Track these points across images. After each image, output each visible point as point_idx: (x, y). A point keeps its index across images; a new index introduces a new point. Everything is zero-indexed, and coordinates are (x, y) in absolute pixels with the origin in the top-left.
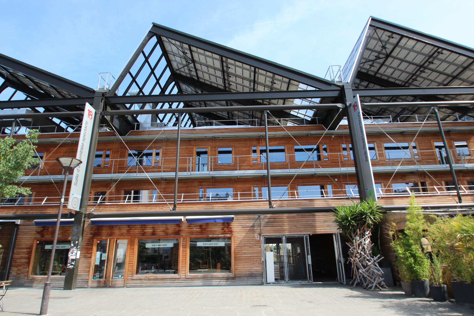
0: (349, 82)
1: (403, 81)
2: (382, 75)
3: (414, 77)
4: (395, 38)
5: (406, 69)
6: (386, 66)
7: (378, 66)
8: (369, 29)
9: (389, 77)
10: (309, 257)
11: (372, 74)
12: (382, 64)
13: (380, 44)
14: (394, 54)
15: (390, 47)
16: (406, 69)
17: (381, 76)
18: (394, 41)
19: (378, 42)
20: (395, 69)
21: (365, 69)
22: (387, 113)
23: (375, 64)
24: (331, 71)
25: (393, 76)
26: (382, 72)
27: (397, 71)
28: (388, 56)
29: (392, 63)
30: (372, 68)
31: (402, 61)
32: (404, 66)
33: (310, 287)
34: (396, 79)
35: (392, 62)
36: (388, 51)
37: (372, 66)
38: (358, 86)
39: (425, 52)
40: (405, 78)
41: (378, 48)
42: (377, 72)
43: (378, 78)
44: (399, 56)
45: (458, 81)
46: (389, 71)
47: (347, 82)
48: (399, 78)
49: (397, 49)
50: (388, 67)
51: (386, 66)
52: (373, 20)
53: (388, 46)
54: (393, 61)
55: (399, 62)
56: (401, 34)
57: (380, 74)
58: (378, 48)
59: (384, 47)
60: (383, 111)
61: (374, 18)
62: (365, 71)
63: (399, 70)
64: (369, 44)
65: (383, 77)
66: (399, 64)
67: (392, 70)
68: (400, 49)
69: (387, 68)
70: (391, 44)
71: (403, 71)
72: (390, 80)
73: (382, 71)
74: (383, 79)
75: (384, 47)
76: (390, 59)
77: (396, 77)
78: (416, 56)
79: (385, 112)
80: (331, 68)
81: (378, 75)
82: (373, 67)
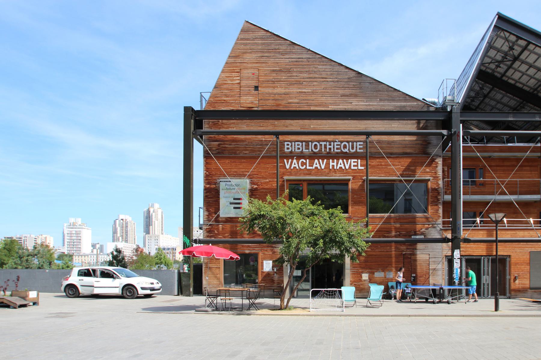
0: (460, 102)
1: (531, 88)
2: (509, 78)
3: (521, 105)
4: (516, 50)
5: (535, 74)
6: (514, 69)
7: (505, 68)
8: (493, 30)
9: (516, 82)
10: (191, 290)
11: (499, 76)
12: (510, 67)
13: (506, 44)
14: (523, 57)
15: (517, 50)
16: (535, 74)
17: (508, 79)
18: (522, 43)
19: (505, 42)
20: (523, 74)
21: (491, 69)
22: (526, 109)
23: (501, 65)
24: (445, 86)
25: (521, 80)
26: (510, 75)
27: (525, 76)
28: (485, 96)
29: (528, 58)
30: (499, 69)
31: (531, 66)
32: (532, 71)
33: (499, 308)
34: (524, 85)
35: (528, 57)
36: (516, 53)
37: (498, 66)
38: (513, 45)
39: (530, 85)
40: (534, 84)
41: (505, 48)
42: (504, 75)
43: (504, 81)
44: (528, 60)
45: (297, 305)
46: (517, 76)
47: (457, 102)
48: (528, 84)
49: (526, 53)
50: (516, 70)
51: (514, 69)
52: (501, 18)
53: (515, 47)
54: (529, 55)
55: (527, 67)
56: (528, 40)
57: (507, 77)
58: (505, 48)
59: (511, 48)
60: (521, 107)
61: (501, 16)
62: (490, 71)
63: (528, 75)
64: (489, 52)
65: (511, 81)
66: (535, 59)
67: (520, 74)
68: (513, 71)
69: (530, 54)
70: (519, 46)
71: (531, 77)
72: (518, 85)
73: (509, 73)
74: (510, 84)
75: (511, 48)
76: (517, 64)
77: (524, 82)
78: (536, 72)
79: (524, 108)
80: (445, 82)
81: (504, 78)
82: (500, 69)
